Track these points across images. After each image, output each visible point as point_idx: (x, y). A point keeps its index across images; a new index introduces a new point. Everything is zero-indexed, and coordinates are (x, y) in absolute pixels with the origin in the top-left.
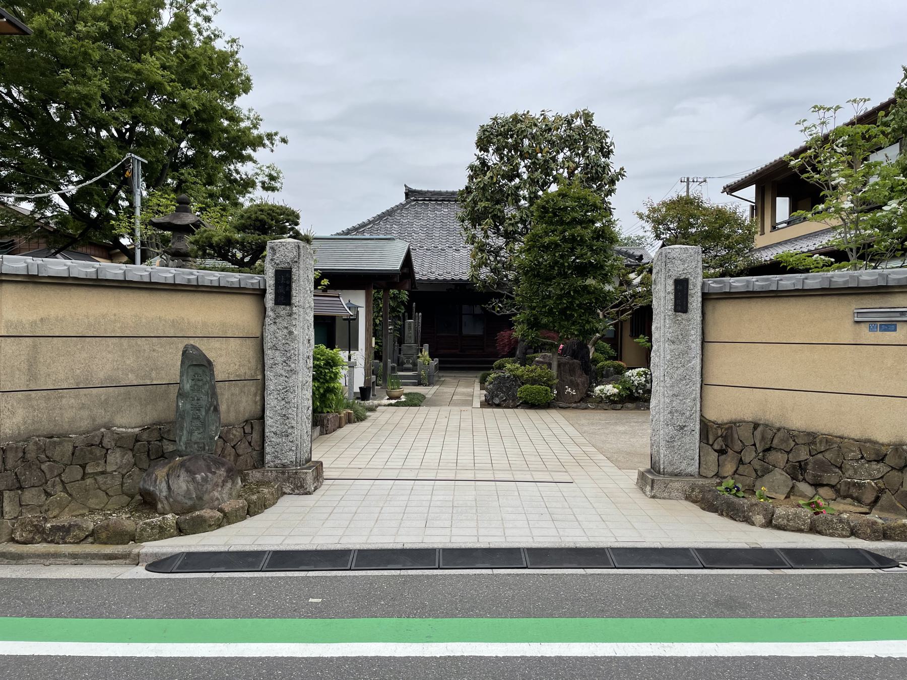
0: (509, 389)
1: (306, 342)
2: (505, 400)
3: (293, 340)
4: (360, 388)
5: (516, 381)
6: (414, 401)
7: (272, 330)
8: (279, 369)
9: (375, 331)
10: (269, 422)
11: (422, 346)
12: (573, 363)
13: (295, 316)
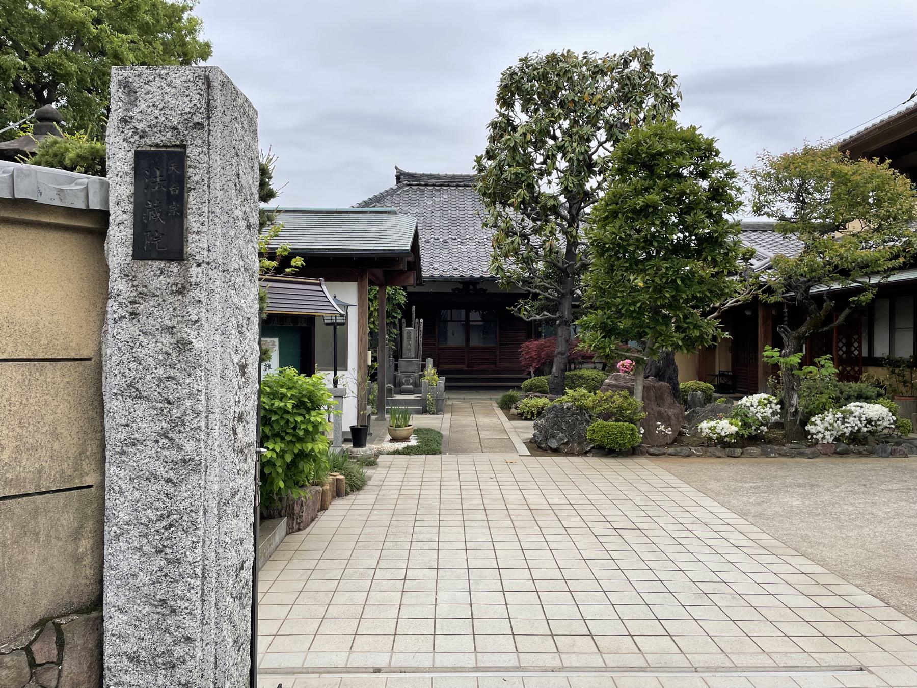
0: (571, 426)
1: (231, 372)
2: (567, 444)
3: (192, 368)
4: (352, 428)
5: (582, 414)
6: (430, 444)
7: (124, 336)
8: (147, 458)
9: (372, 340)
10: (115, 623)
11: (424, 360)
12: (660, 388)
13: (196, 294)
